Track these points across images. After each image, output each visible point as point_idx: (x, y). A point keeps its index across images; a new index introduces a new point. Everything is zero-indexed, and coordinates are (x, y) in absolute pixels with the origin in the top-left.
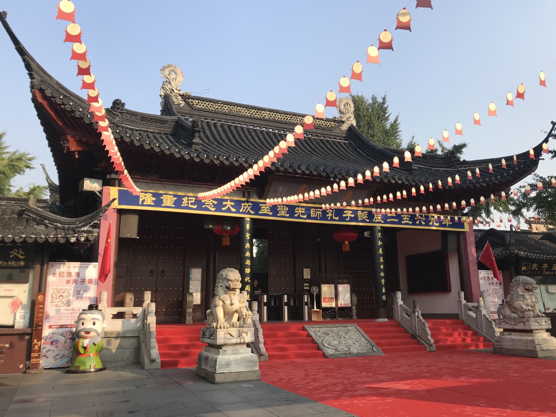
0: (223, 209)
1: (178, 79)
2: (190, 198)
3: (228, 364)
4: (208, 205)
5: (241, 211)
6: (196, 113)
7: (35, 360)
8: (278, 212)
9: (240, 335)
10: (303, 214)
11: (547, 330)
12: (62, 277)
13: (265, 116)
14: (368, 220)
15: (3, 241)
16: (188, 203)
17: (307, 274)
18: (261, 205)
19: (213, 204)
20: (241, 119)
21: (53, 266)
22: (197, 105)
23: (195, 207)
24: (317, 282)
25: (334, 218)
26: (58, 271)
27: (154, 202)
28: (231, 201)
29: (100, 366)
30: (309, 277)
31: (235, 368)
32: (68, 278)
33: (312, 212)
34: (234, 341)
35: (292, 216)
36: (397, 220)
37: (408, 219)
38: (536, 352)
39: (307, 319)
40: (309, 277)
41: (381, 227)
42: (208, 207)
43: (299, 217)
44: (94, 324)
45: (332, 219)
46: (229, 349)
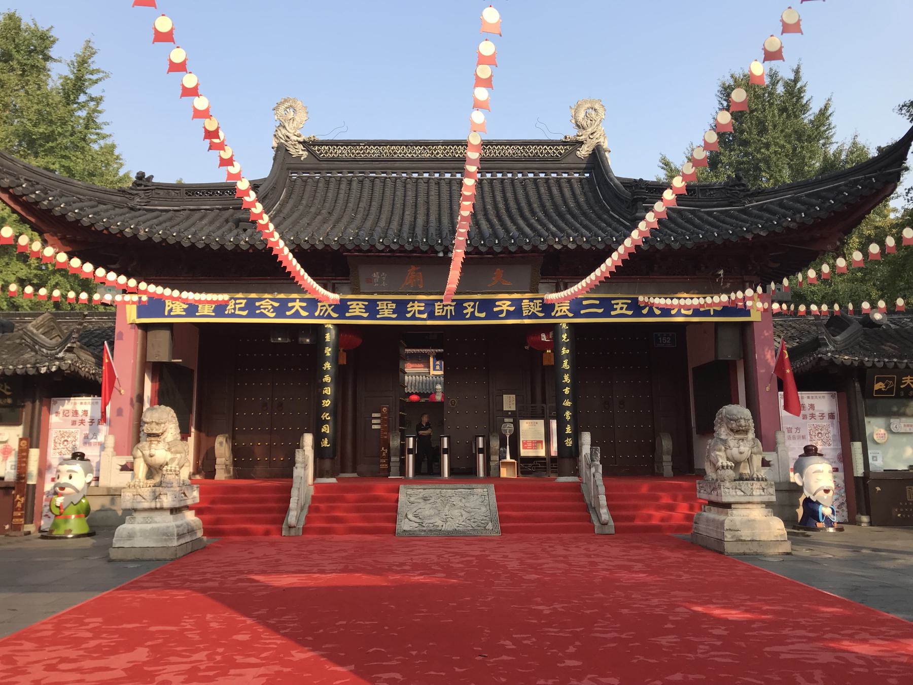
0: (288, 313)
1: (297, 118)
2: (238, 301)
3: (131, 536)
4: (265, 309)
5: (317, 314)
6: (324, 165)
7: (17, 520)
8: (378, 312)
9: (156, 497)
10: (420, 312)
11: (768, 505)
12: (69, 417)
13: (438, 153)
14: (541, 315)
15: (4, 374)
16: (235, 309)
17: (509, 403)
18: (349, 303)
19: (273, 307)
20: (397, 165)
21: (55, 403)
22: (326, 153)
23: (245, 313)
24: (517, 417)
25: (477, 314)
26: (61, 409)
27: (185, 310)
28: (301, 300)
29: (86, 530)
30: (513, 408)
31: (139, 542)
32: (74, 418)
33: (437, 307)
34: (146, 505)
35: (401, 316)
36: (601, 311)
37: (625, 306)
38: (721, 541)
39: (482, 474)
40: (513, 408)
41: (568, 324)
42: (265, 312)
43: (413, 318)
44: (70, 477)
45: (473, 317)
46: (139, 516)
